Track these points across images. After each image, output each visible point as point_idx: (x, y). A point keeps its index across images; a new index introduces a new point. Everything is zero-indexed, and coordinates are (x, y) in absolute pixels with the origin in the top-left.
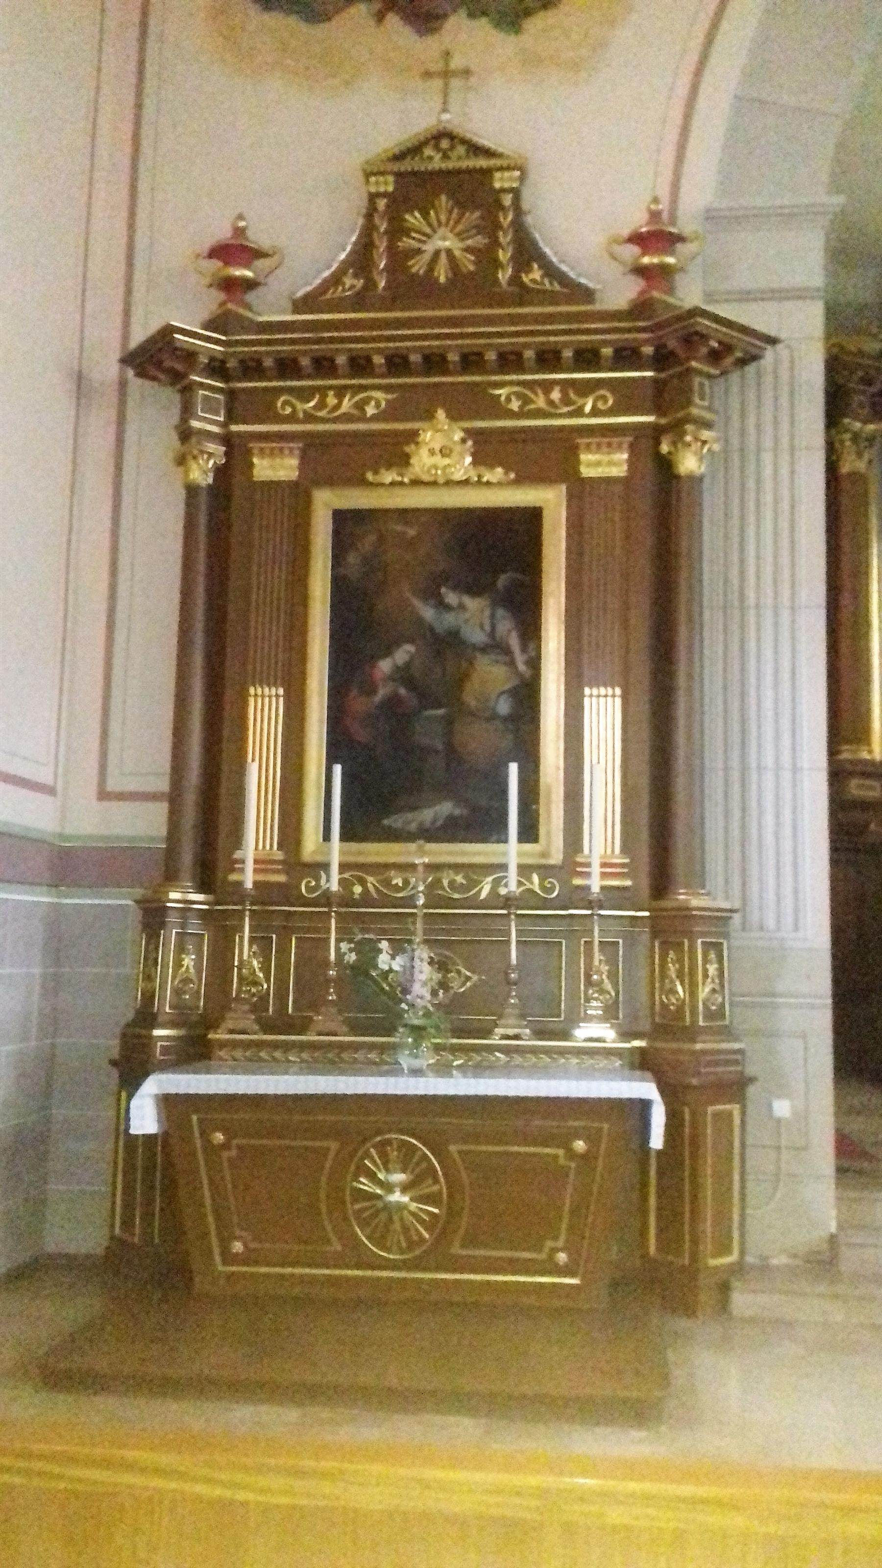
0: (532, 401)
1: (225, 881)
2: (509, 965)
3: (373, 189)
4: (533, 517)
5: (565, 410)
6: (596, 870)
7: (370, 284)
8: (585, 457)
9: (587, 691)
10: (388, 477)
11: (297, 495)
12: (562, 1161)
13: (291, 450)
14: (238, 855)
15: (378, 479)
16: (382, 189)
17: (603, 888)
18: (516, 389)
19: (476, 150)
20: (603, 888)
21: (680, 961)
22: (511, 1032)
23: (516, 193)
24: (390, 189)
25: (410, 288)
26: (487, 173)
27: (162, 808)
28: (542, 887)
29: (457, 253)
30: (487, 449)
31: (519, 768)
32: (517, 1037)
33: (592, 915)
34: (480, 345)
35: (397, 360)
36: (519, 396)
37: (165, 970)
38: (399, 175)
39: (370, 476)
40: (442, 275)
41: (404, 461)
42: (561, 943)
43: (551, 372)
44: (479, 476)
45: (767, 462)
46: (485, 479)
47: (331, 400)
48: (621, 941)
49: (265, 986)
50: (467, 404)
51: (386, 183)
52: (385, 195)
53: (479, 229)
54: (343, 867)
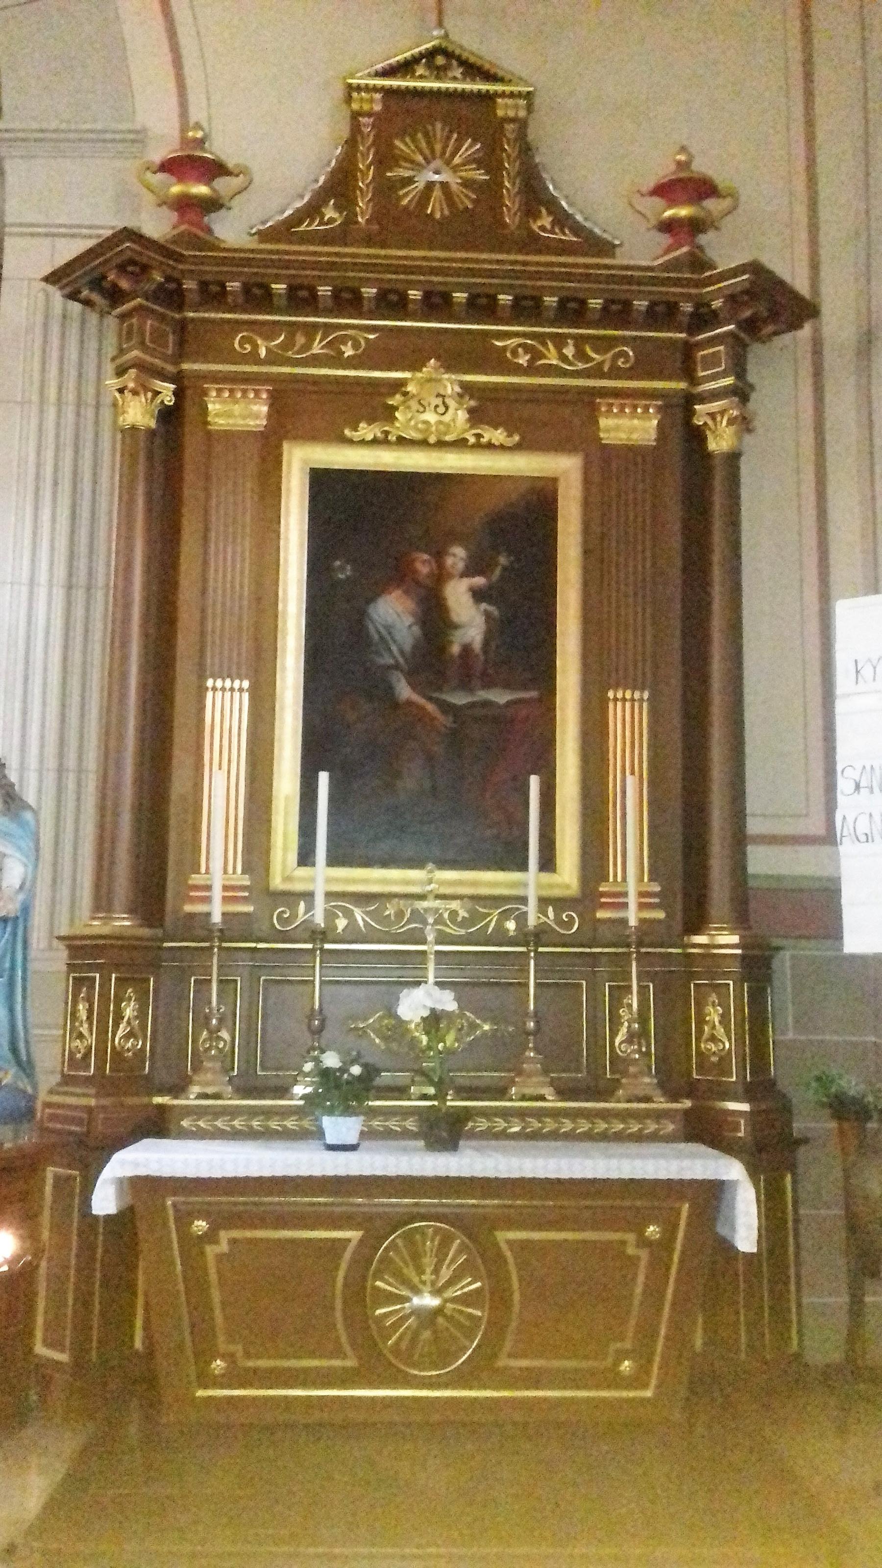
0: (543, 356)
1: (177, 910)
2: (526, 1014)
3: (355, 106)
4: (322, 481)
5: (581, 366)
6: (217, 894)
7: (350, 220)
8: (603, 422)
9: (210, 683)
10: (366, 431)
11: (268, 447)
12: (631, 1251)
13: (257, 393)
14: (195, 879)
15: (356, 435)
16: (366, 107)
17: (642, 921)
18: (521, 340)
19: (473, 70)
20: (642, 921)
21: (89, 1000)
22: (210, 1090)
23: (523, 125)
24: (378, 108)
25: (396, 222)
26: (488, 98)
27: (754, 826)
28: (559, 921)
29: (454, 187)
30: (486, 407)
31: (331, 777)
32: (217, 1096)
33: (313, 950)
34: (674, 294)
35: (437, 300)
36: (527, 348)
37: (249, 1029)
38: (389, 93)
39: (347, 432)
40: (436, 207)
41: (389, 414)
42: (236, 981)
43: (401, 320)
44: (478, 436)
45: (106, 428)
46: (484, 440)
47: (300, 340)
48: (731, 983)
49: (727, 1046)
50: (460, 355)
51: (372, 101)
52: (369, 115)
53: (480, 163)
54: (329, 895)
